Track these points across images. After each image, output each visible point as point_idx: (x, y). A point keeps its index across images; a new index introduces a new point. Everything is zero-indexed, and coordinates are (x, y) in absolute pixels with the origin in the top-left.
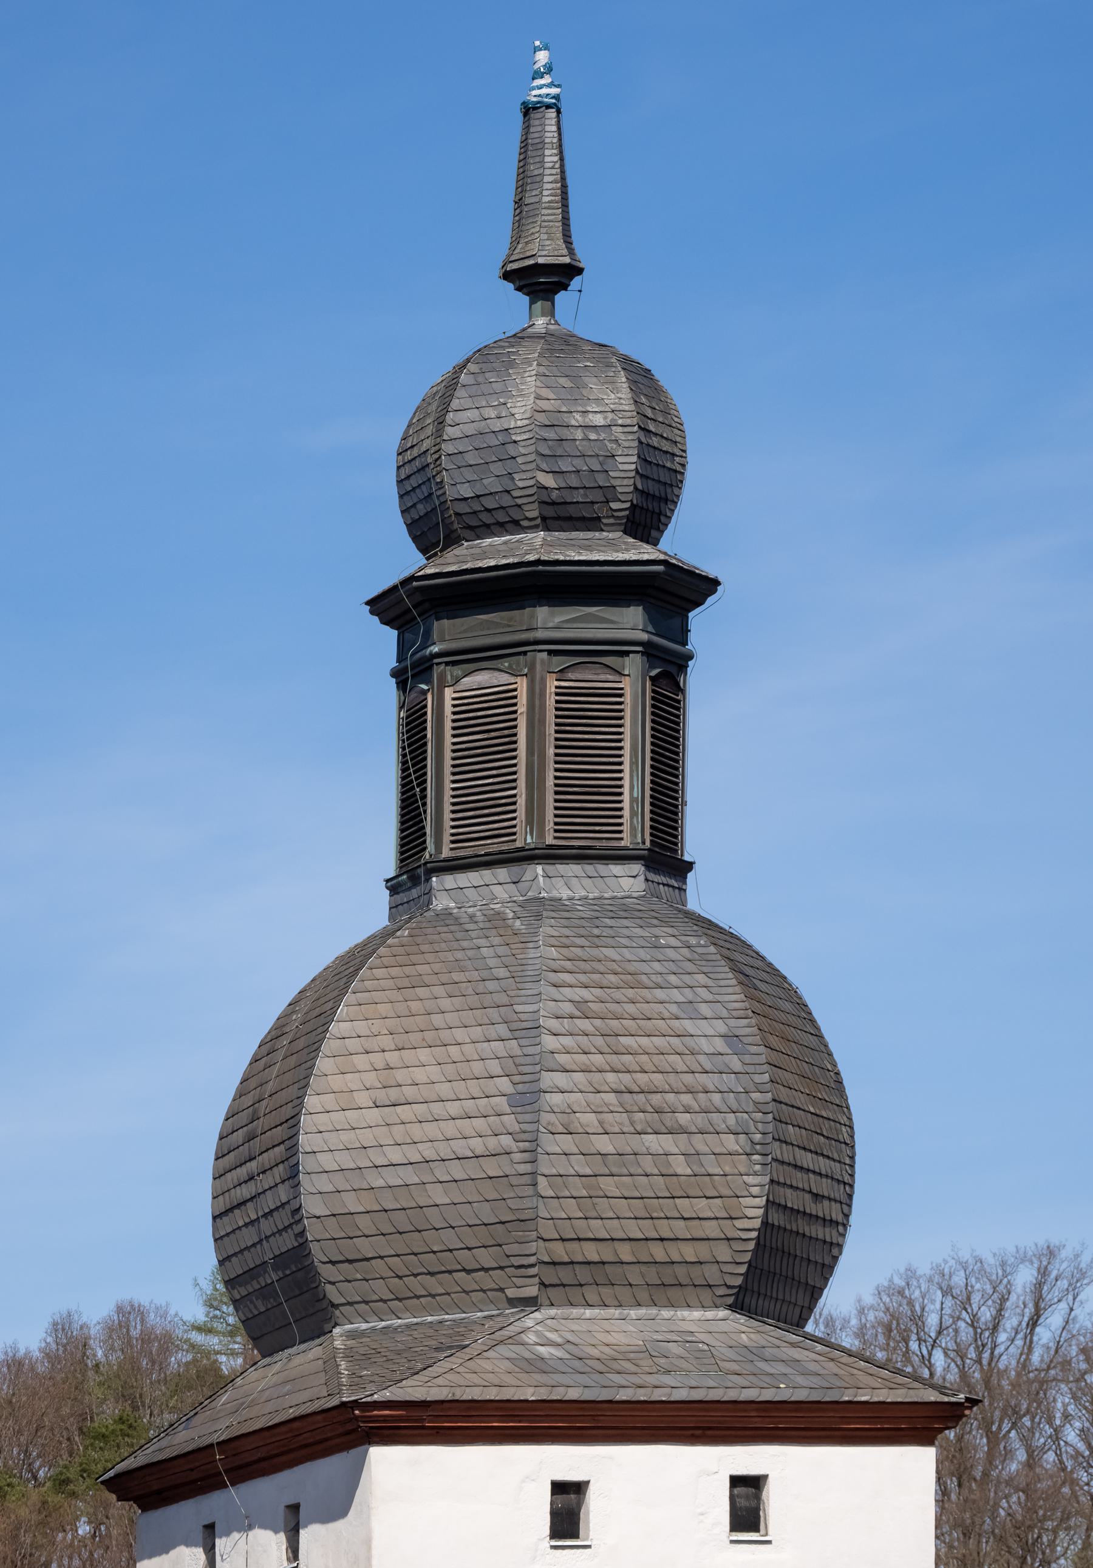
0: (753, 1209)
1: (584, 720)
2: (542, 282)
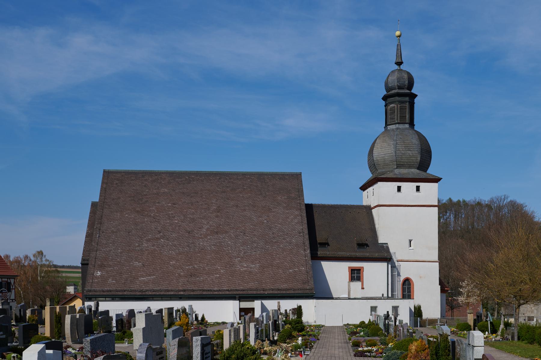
0: (419, 159)
1: (402, 109)
2: (399, 64)
